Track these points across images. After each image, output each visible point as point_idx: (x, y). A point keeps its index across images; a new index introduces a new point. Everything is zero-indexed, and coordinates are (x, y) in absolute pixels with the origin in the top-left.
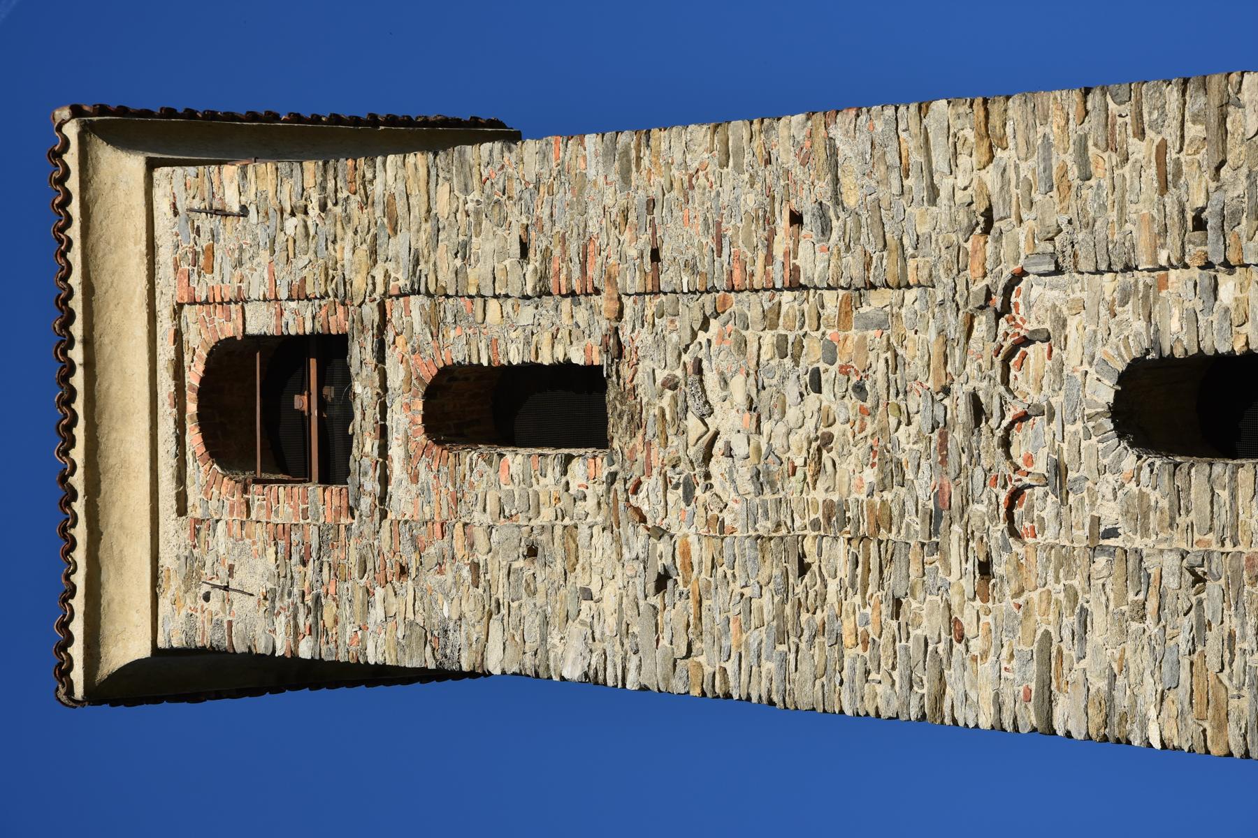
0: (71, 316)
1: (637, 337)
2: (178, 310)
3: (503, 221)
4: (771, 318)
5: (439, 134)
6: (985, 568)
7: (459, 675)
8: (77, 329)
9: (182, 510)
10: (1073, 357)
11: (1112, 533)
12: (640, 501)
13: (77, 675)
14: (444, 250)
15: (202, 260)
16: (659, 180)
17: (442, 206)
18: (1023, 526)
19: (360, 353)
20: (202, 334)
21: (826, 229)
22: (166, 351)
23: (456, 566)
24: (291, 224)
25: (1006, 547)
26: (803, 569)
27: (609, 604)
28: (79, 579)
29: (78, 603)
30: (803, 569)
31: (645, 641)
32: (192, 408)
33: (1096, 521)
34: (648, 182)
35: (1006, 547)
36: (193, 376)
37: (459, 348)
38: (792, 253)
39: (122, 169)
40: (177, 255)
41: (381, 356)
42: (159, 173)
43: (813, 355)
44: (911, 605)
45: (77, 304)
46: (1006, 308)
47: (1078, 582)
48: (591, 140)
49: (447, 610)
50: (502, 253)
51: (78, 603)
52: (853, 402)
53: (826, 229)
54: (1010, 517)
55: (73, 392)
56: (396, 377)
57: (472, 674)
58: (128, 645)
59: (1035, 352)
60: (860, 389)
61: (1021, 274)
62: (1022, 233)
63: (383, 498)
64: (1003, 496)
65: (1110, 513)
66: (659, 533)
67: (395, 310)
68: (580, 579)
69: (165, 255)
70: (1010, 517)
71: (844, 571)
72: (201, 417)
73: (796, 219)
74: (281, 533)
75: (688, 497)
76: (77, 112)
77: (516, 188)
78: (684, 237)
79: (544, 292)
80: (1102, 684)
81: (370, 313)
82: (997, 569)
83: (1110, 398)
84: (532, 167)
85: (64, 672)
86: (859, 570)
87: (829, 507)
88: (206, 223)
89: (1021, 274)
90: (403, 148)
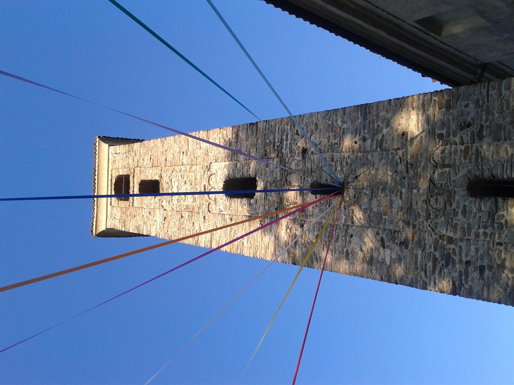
0: (96, 171)
1: (164, 175)
2: (112, 170)
3: (148, 154)
4: (180, 170)
5: (138, 141)
6: (204, 217)
7: (143, 235)
8: (96, 173)
9: (111, 205)
10: (218, 178)
11: (222, 211)
12: (163, 204)
13: (94, 231)
14: (140, 160)
15: (114, 162)
16: (167, 146)
17: (141, 152)
18: (210, 210)
19: (131, 178)
20: (115, 174)
21: (187, 155)
22: (110, 178)
23: (148, 217)
24: (125, 155)
25: (207, 213)
26: (182, 217)
27: (158, 223)
28: (95, 215)
29: (95, 219)
30: (182, 217)
31: (162, 229)
32: (113, 187)
33: (220, 209)
34: (166, 147)
35: (207, 213)
36: (114, 182)
37: (144, 178)
38: (182, 159)
39: (105, 146)
40: (111, 161)
41: (133, 178)
42: (110, 147)
43: (185, 179)
44: (195, 224)
45: (97, 169)
46: (210, 168)
47: (216, 220)
48: (159, 139)
49: (139, 223)
50: (148, 160)
51: (95, 219)
52: (190, 186)
53: (187, 155)
54: (208, 208)
55: (95, 183)
56: (135, 182)
57: (147, 236)
58: (102, 228)
59: (213, 176)
60: (191, 184)
61: (211, 163)
62: (212, 155)
63: (133, 203)
64: (208, 204)
65: (222, 208)
66: (165, 210)
67: (136, 169)
68: (155, 218)
69: (110, 161)
70: (208, 208)
71: (187, 218)
72: (114, 189)
73: (183, 153)
74: (121, 208)
75: (169, 204)
76: (99, 137)
77: (150, 148)
78: (170, 157)
79: (153, 167)
80: (218, 239)
81: (132, 171)
82: (206, 218)
83: (222, 186)
84: (152, 145)
85: (92, 231)
86: (463, 277)
87: (187, 205)
88: (115, 155)
89: (211, 163)
90: (137, 142)
